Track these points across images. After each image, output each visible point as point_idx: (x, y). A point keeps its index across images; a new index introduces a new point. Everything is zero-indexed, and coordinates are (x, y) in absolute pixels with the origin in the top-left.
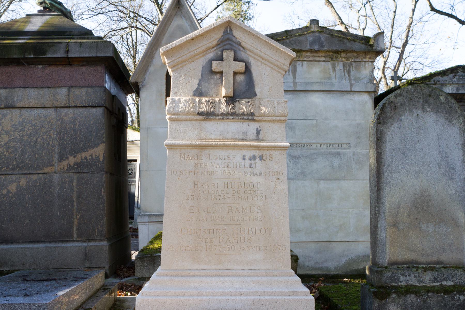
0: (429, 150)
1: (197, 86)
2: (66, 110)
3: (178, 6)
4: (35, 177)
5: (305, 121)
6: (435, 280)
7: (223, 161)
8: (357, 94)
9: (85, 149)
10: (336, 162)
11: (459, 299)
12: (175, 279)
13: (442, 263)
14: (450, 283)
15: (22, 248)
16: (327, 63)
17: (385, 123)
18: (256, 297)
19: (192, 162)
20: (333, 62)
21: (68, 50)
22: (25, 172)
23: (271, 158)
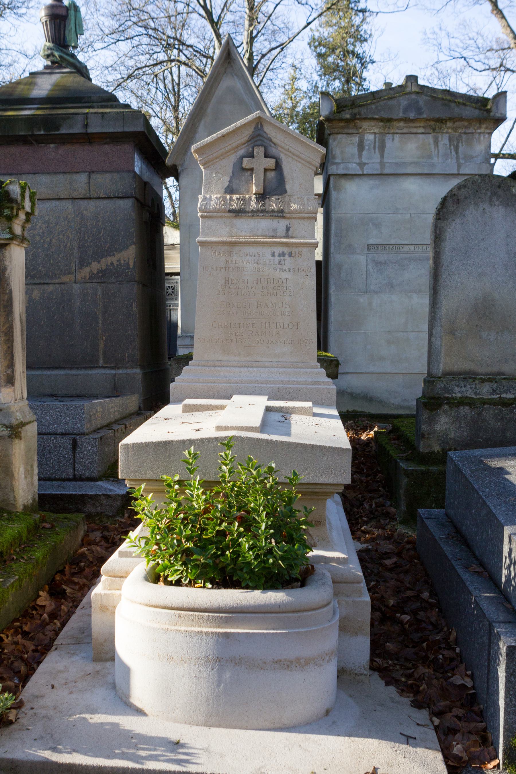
0: (495, 249)
1: (228, 183)
2: (86, 202)
3: (228, 61)
4: (51, 288)
5: (394, 215)
6: (494, 391)
7: (253, 258)
9: (110, 252)
12: (207, 368)
13: (504, 375)
14: (510, 396)
15: (37, 375)
16: (427, 135)
18: (281, 386)
19: (223, 258)
20: (435, 134)
21: (87, 124)
22: (38, 282)
23: (300, 255)
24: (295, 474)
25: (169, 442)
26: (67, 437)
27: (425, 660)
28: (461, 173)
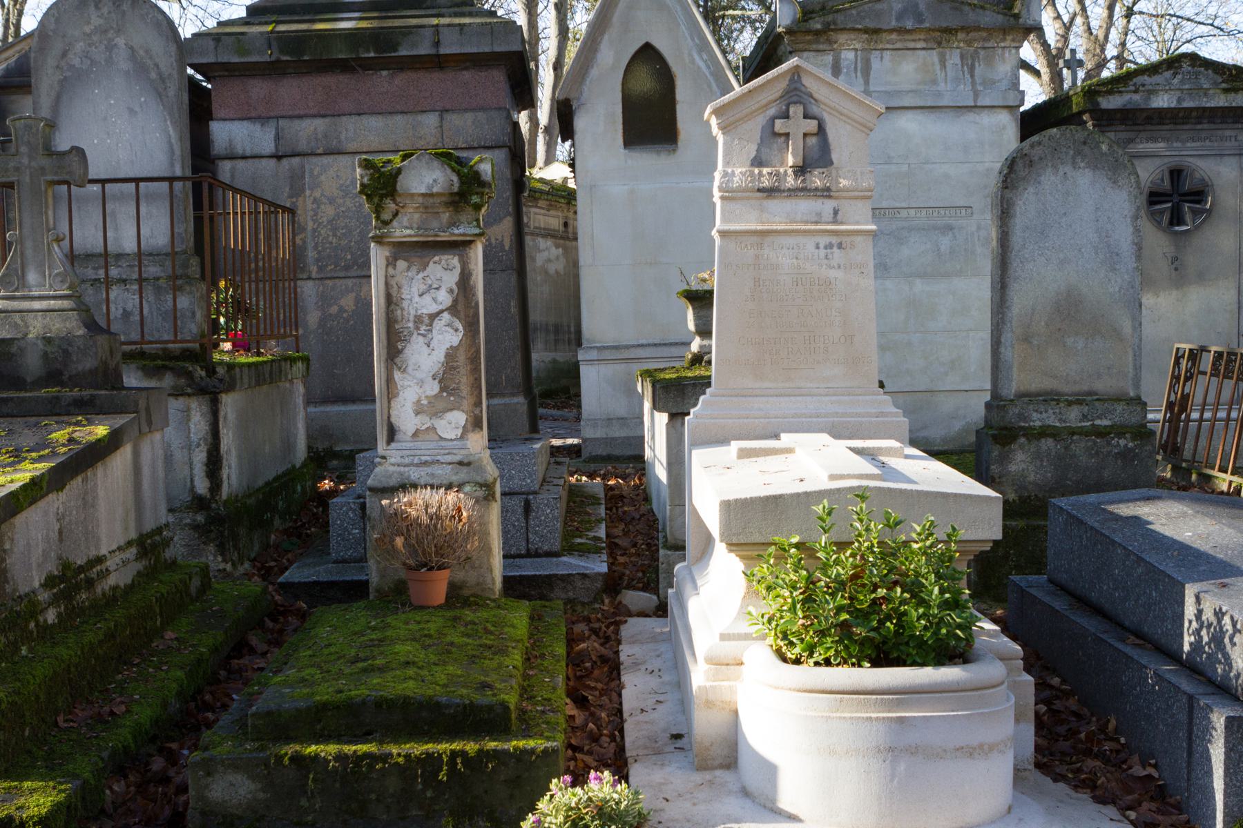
8: (986, 111)
10: (945, 242)
11: (1118, 445)
14: (1106, 422)
17: (1014, 188)
23: (853, 246)
24: (954, 529)
25: (781, 496)
26: (515, 498)
27: (1088, 753)
28: (979, 104)
